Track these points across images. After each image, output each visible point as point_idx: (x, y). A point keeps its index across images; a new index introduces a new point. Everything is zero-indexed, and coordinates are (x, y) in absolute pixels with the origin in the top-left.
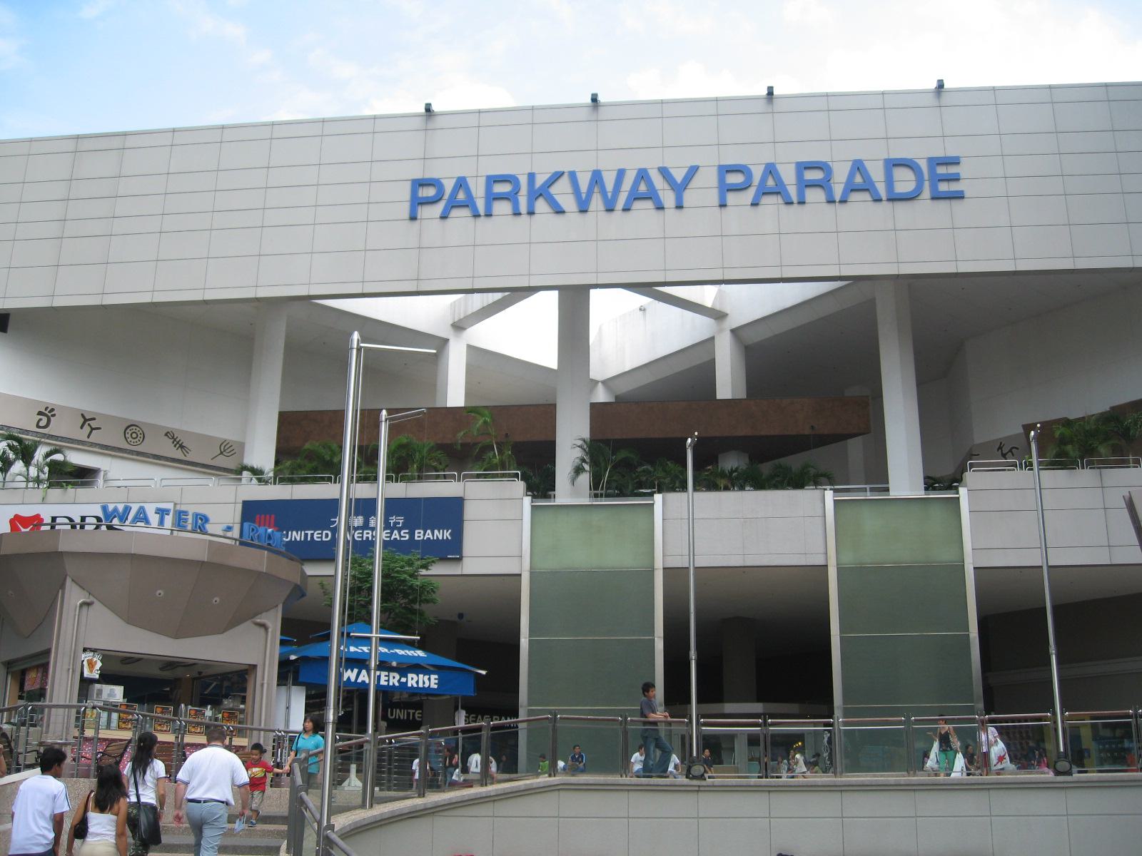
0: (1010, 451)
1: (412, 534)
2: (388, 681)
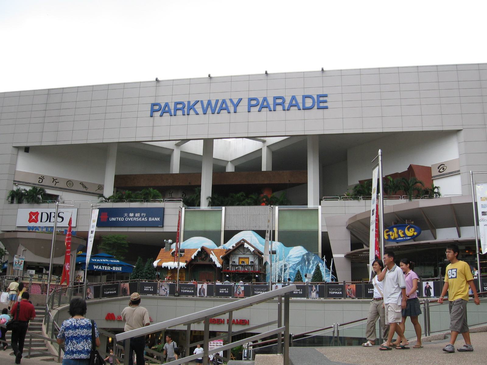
1: (148, 219)
2: (107, 269)
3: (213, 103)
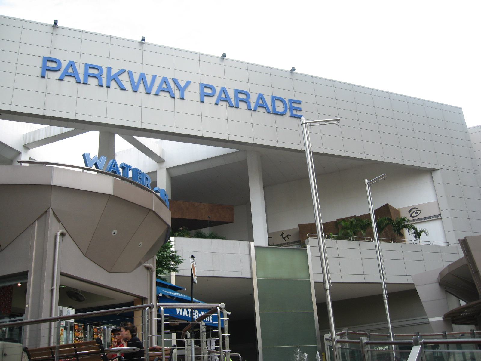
0: (287, 236)
3: (149, 80)
